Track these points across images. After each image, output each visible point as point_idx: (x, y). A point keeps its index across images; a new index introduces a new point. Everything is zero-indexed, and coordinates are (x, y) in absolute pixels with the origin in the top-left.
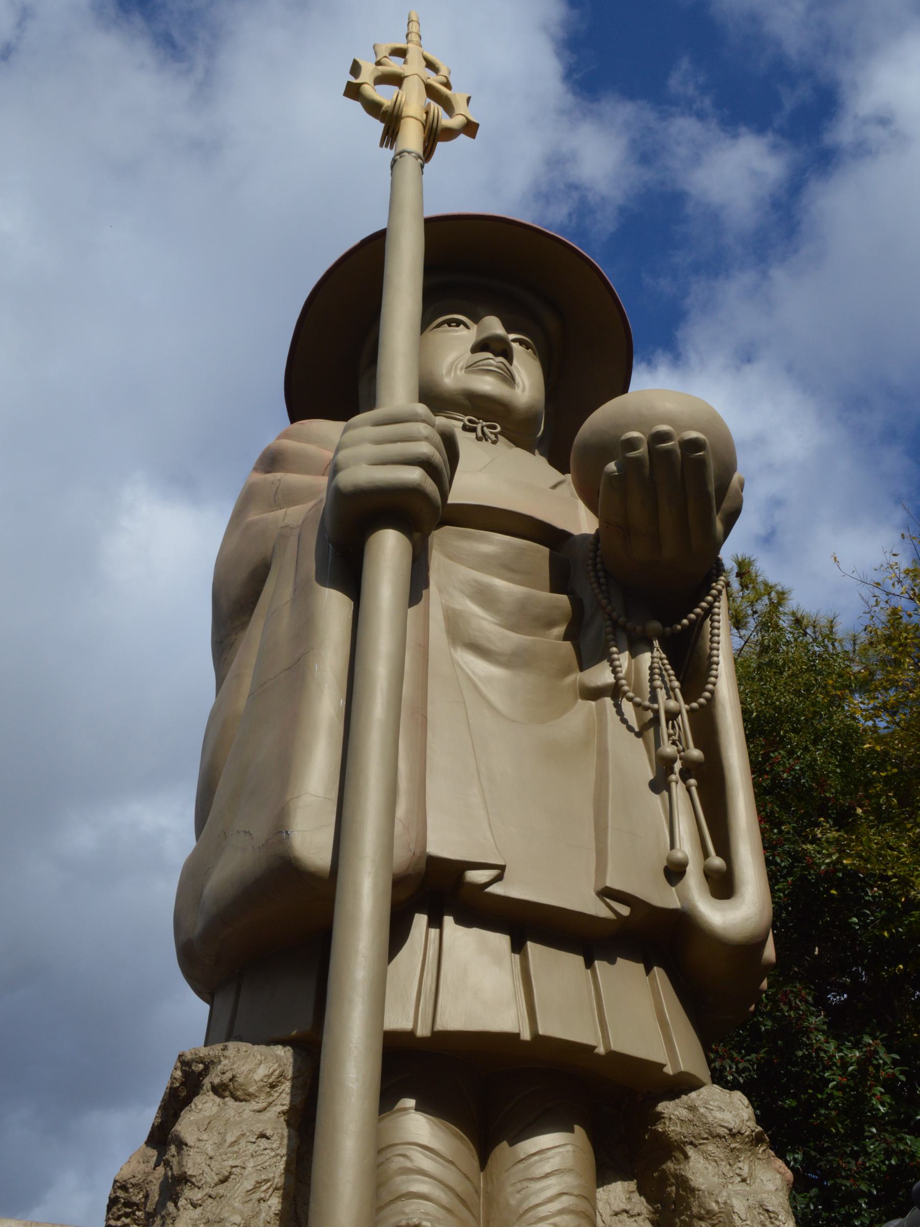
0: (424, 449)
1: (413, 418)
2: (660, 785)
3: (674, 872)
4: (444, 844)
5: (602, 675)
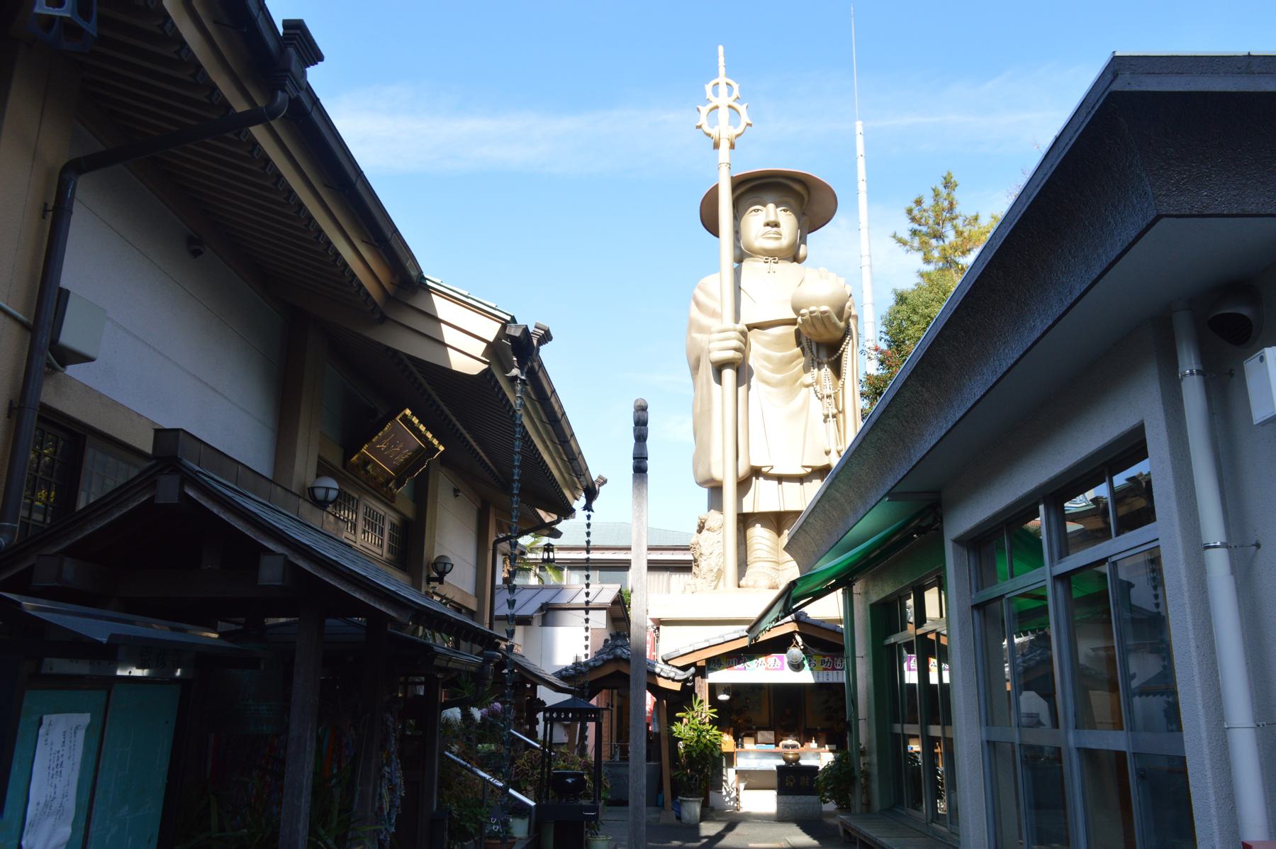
0: (736, 343)
1: (737, 318)
2: (825, 421)
3: (827, 453)
4: (756, 463)
5: (807, 378)
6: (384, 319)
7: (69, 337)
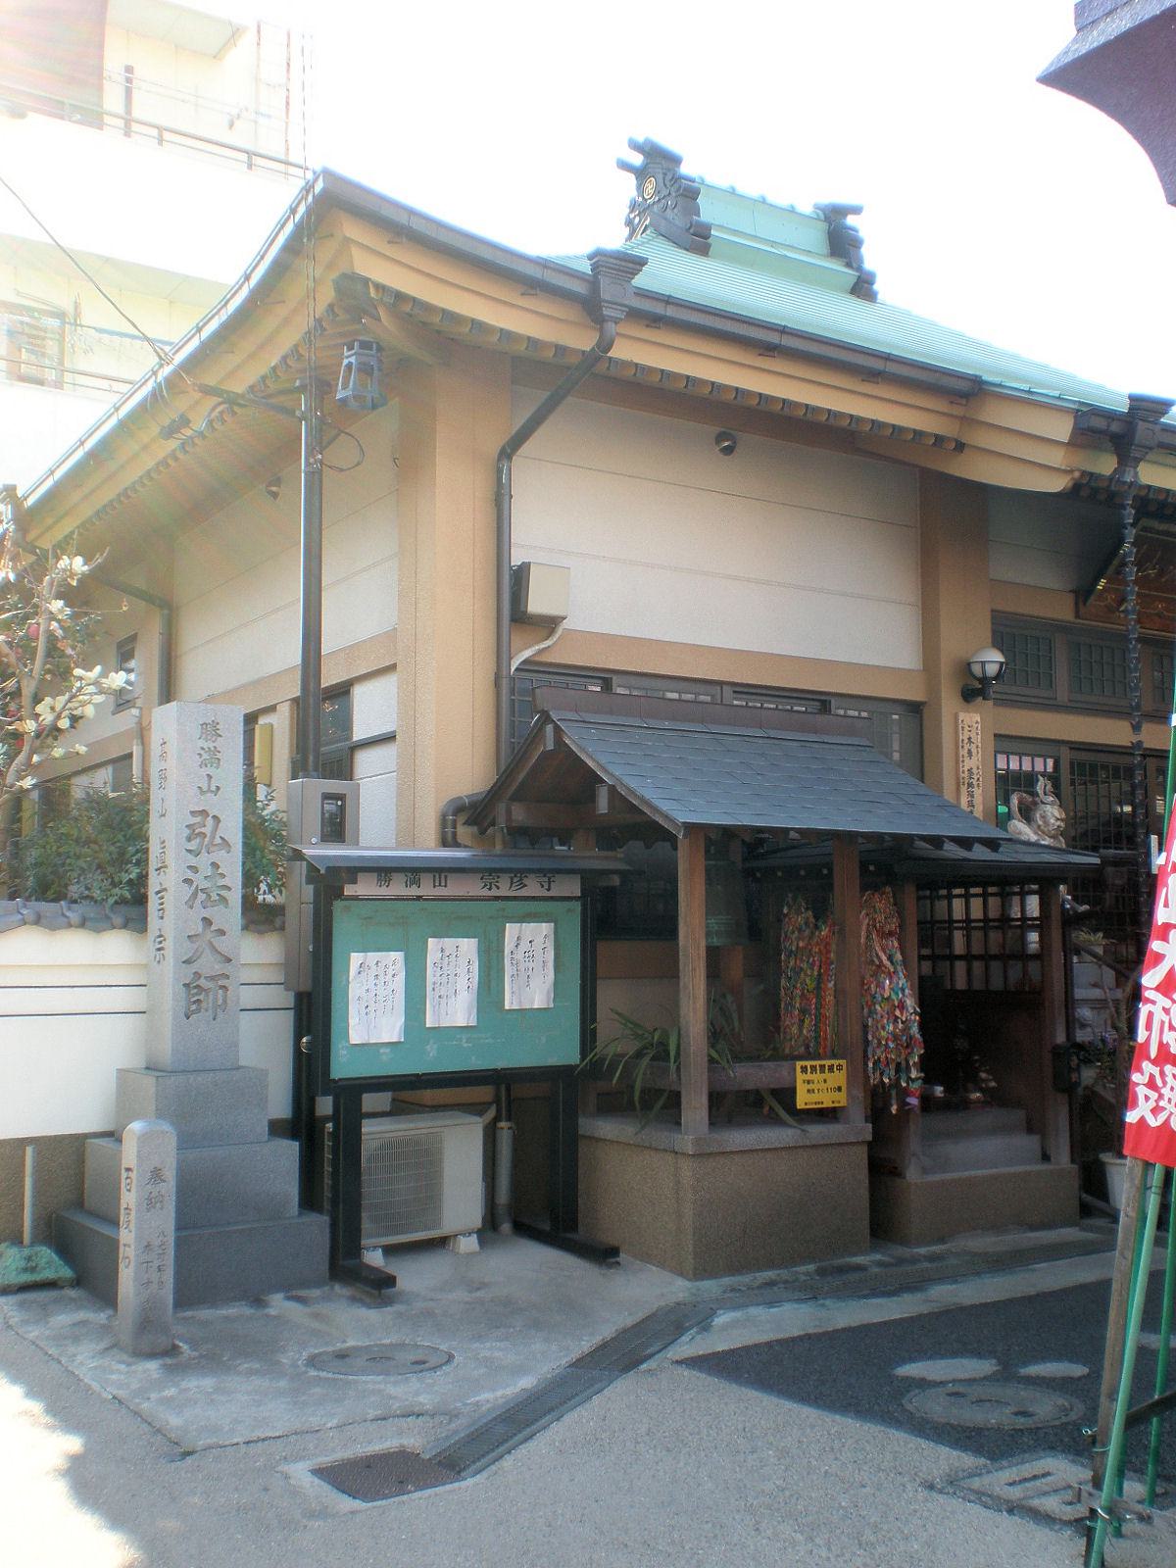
6: (960, 447)
7: (536, 605)
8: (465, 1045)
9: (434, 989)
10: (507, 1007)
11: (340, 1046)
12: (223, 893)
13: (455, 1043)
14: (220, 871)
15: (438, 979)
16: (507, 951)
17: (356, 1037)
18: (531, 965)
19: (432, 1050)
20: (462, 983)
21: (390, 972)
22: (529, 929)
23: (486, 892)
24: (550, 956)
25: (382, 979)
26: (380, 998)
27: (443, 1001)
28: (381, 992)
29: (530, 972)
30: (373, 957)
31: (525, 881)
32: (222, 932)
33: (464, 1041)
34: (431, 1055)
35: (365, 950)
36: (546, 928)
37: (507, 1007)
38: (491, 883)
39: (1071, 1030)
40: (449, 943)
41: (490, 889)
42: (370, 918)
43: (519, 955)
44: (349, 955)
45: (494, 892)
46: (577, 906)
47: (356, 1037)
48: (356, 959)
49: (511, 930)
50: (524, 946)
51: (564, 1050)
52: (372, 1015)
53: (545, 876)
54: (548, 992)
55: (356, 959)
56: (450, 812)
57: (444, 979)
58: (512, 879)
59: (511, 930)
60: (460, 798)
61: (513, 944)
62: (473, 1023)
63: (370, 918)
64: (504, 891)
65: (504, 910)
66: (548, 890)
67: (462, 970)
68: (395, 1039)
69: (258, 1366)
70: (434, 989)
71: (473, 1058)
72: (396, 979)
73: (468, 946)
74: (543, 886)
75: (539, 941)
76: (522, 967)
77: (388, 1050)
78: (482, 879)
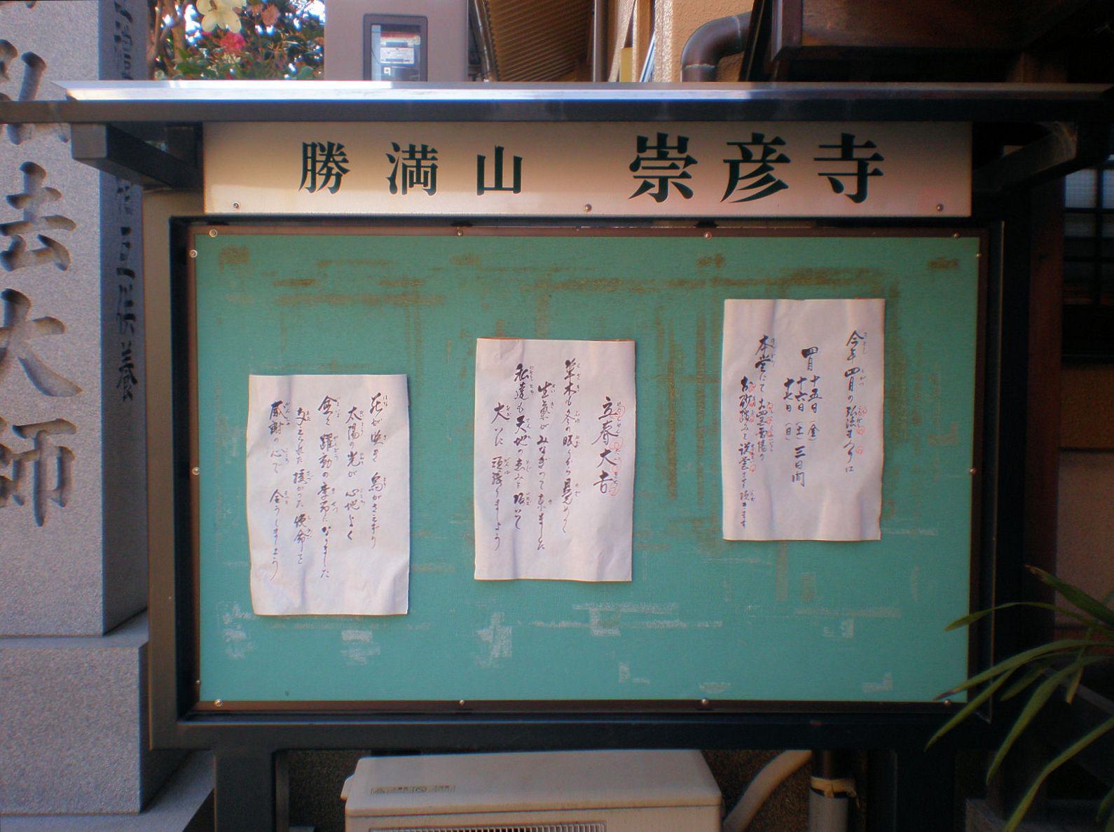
8: (597, 632)
9: (497, 478)
10: (729, 533)
11: (228, 619)
12: (54, 234)
13: (564, 624)
14: (46, 183)
15: (509, 451)
16: (729, 376)
17: (271, 594)
18: (807, 419)
19: (497, 640)
20: (585, 464)
21: (366, 428)
22: (801, 317)
23: (646, 206)
24: (871, 394)
25: (343, 446)
26: (337, 497)
27: (529, 512)
28: (341, 483)
29: (804, 440)
30: (310, 388)
31: (778, 172)
32: (52, 323)
33: (595, 620)
34: (495, 653)
35: (288, 368)
36: (856, 315)
37: (729, 533)
38: (663, 182)
39: (807, 222)
40: (543, 354)
41: (661, 197)
42: (306, 283)
43: (769, 389)
44: (248, 378)
45: (675, 206)
46: (967, 251)
47: (271, 594)
48: (263, 389)
49: (741, 320)
50: (785, 363)
51: (914, 654)
52: (315, 541)
53: (847, 156)
54: (860, 499)
55: (263, 389)
56: (698, 56)
57: (530, 452)
58: (734, 166)
59: (741, 320)
60: (727, 21)
61: (751, 350)
62: (618, 570)
63: (306, 283)
64: (708, 200)
65: (719, 260)
66: (859, 197)
67: (586, 427)
68: (376, 607)
69: (812, 722)
70: (497, 478)
71: (624, 667)
72: (382, 448)
73: (603, 365)
74: (837, 187)
75: (833, 352)
76: (777, 426)
77: (365, 635)
78: (635, 167)
